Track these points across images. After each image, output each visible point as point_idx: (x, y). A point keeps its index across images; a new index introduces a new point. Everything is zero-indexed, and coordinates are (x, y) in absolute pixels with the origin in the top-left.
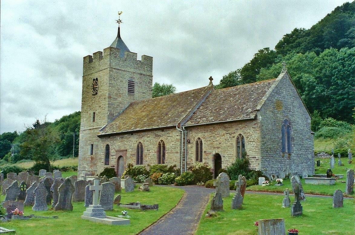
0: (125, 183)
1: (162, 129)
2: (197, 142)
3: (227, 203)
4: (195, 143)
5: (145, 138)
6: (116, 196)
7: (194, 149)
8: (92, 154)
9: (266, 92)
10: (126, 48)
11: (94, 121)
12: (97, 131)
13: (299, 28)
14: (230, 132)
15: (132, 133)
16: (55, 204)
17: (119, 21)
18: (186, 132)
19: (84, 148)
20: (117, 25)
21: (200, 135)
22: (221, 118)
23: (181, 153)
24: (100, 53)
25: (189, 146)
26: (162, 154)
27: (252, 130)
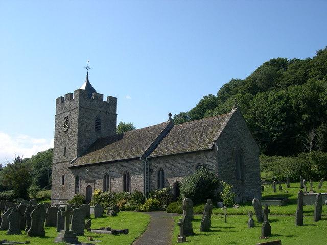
0: (94, 209)
1: (127, 161)
2: (159, 171)
3: (196, 226)
4: (157, 172)
5: (111, 169)
6: (87, 221)
7: (156, 179)
8: (63, 184)
9: (221, 125)
10: (94, 91)
11: (65, 155)
12: (68, 163)
13: (235, 78)
14: (190, 161)
15: (99, 164)
16: (28, 229)
17: (88, 68)
18: (149, 162)
19: (56, 180)
20: (86, 71)
21: (162, 165)
22: (181, 149)
23: (144, 182)
24: (71, 95)
25: (152, 175)
26: (126, 183)
27: (210, 159)
